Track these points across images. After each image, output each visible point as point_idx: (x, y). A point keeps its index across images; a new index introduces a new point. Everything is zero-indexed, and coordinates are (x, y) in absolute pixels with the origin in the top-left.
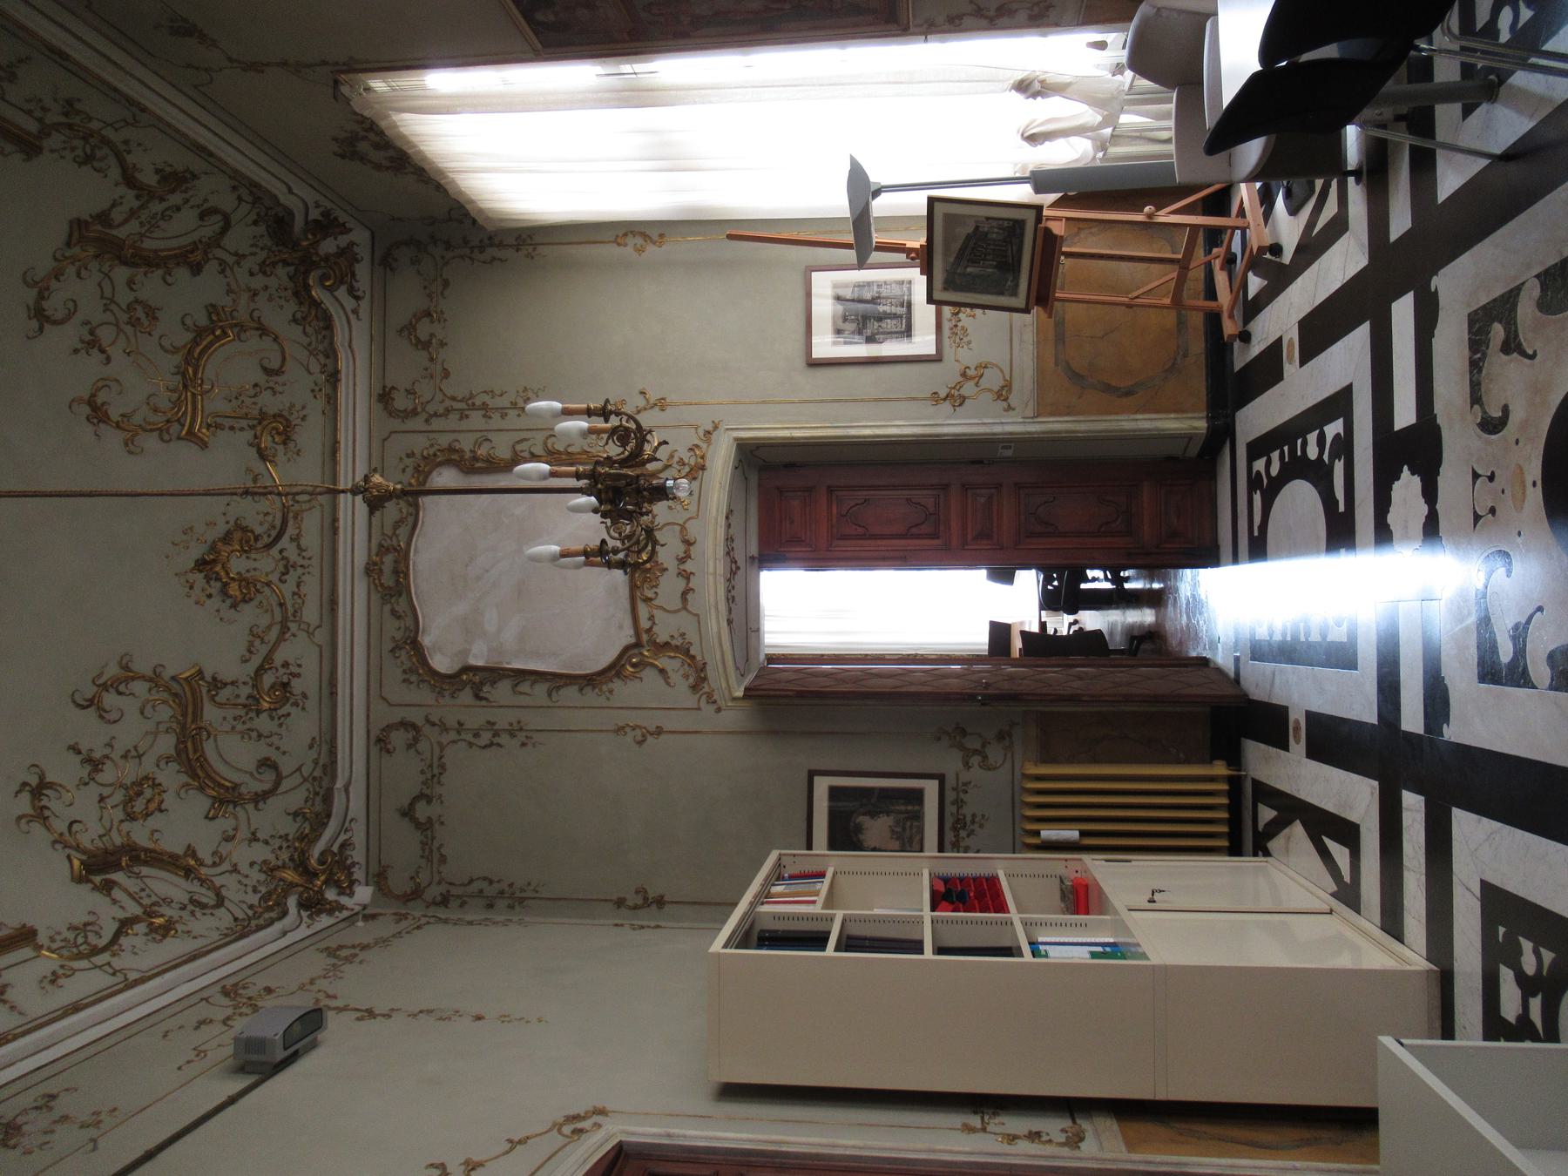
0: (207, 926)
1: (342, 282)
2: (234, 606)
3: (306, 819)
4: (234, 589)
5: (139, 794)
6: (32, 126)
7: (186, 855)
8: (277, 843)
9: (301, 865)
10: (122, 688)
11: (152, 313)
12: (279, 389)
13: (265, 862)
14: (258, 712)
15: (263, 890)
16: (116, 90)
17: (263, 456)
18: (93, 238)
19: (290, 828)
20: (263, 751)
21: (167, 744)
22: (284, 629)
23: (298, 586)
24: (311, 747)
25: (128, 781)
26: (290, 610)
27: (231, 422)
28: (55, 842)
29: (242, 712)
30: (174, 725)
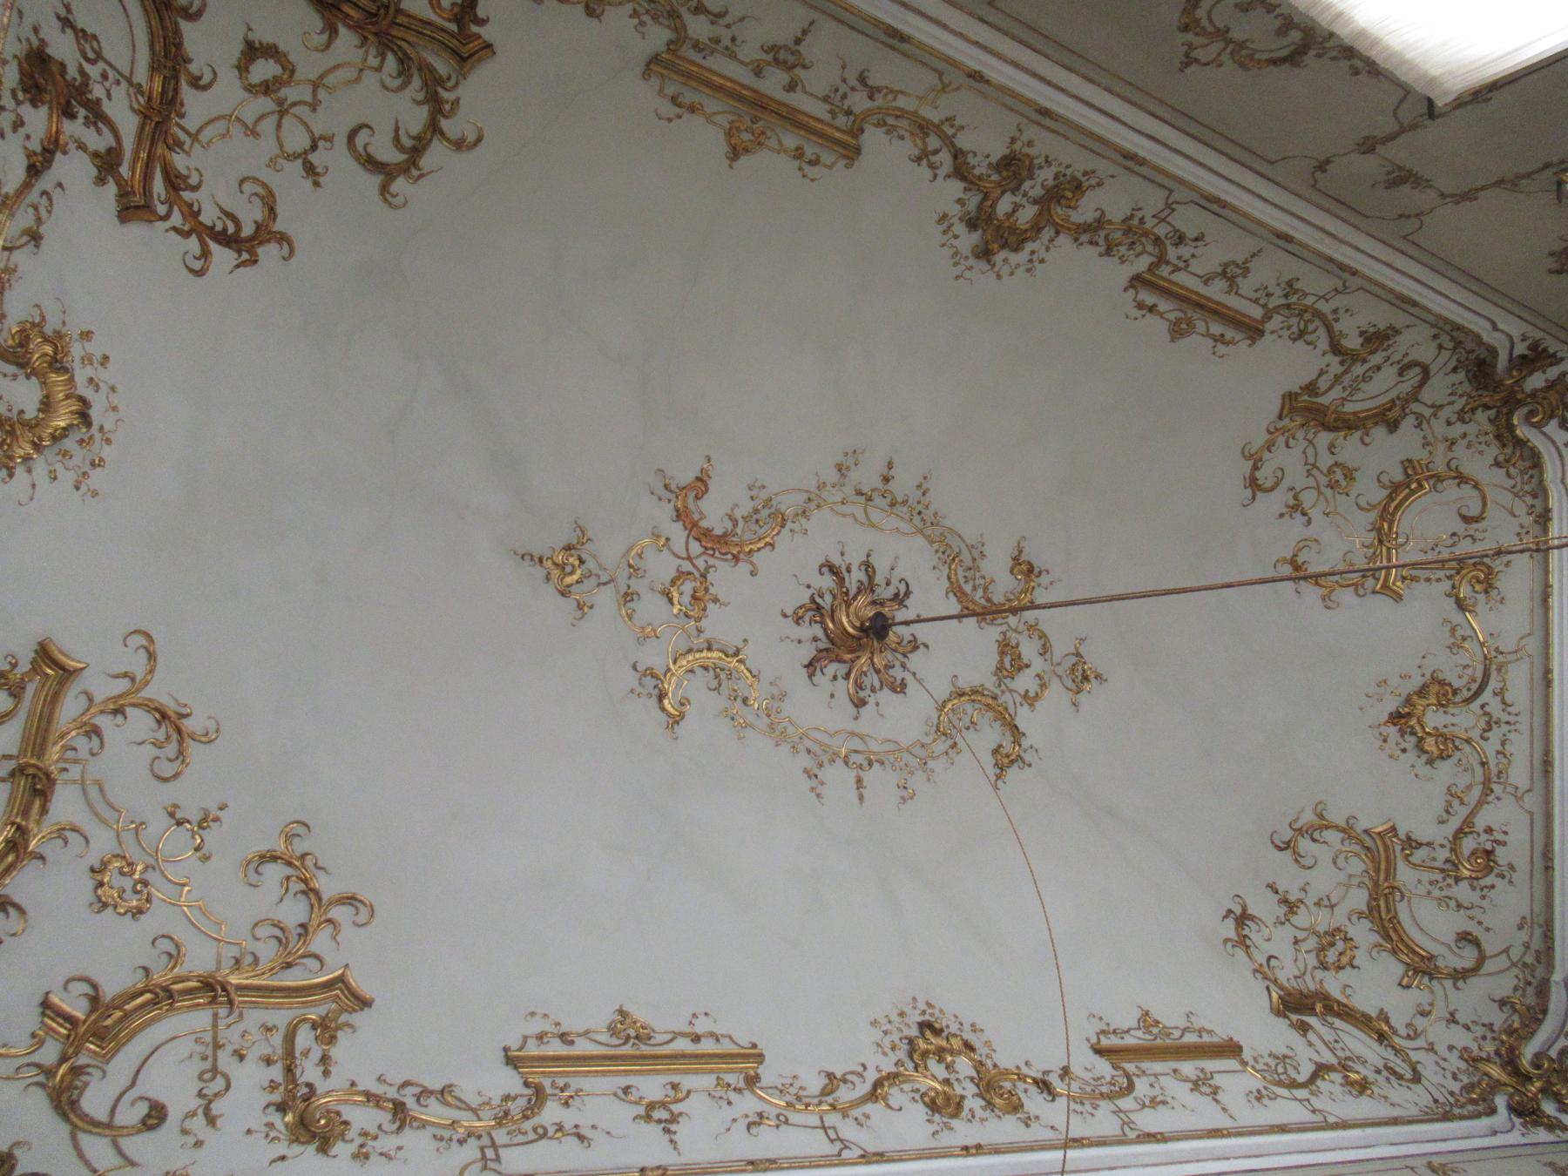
0: (1409, 1099)
1: (1552, 417)
2: (1430, 762)
3: (1515, 1011)
4: (1430, 744)
5: (1332, 945)
6: (1256, 313)
7: (1378, 1018)
8: (1480, 1031)
9: (1510, 1061)
10: (1316, 835)
11: (1349, 474)
12: (1478, 535)
13: (1465, 1049)
14: (1457, 880)
15: (1466, 1080)
16: (1331, 260)
17: (1461, 605)
18: (1305, 410)
19: (1498, 1018)
20: (1461, 923)
21: (1359, 898)
22: (1487, 790)
23: (1503, 744)
24: (1520, 927)
25: (1321, 929)
26: (1494, 771)
27: (1427, 574)
28: (1256, 971)
29: (1439, 877)
30: (1366, 880)
